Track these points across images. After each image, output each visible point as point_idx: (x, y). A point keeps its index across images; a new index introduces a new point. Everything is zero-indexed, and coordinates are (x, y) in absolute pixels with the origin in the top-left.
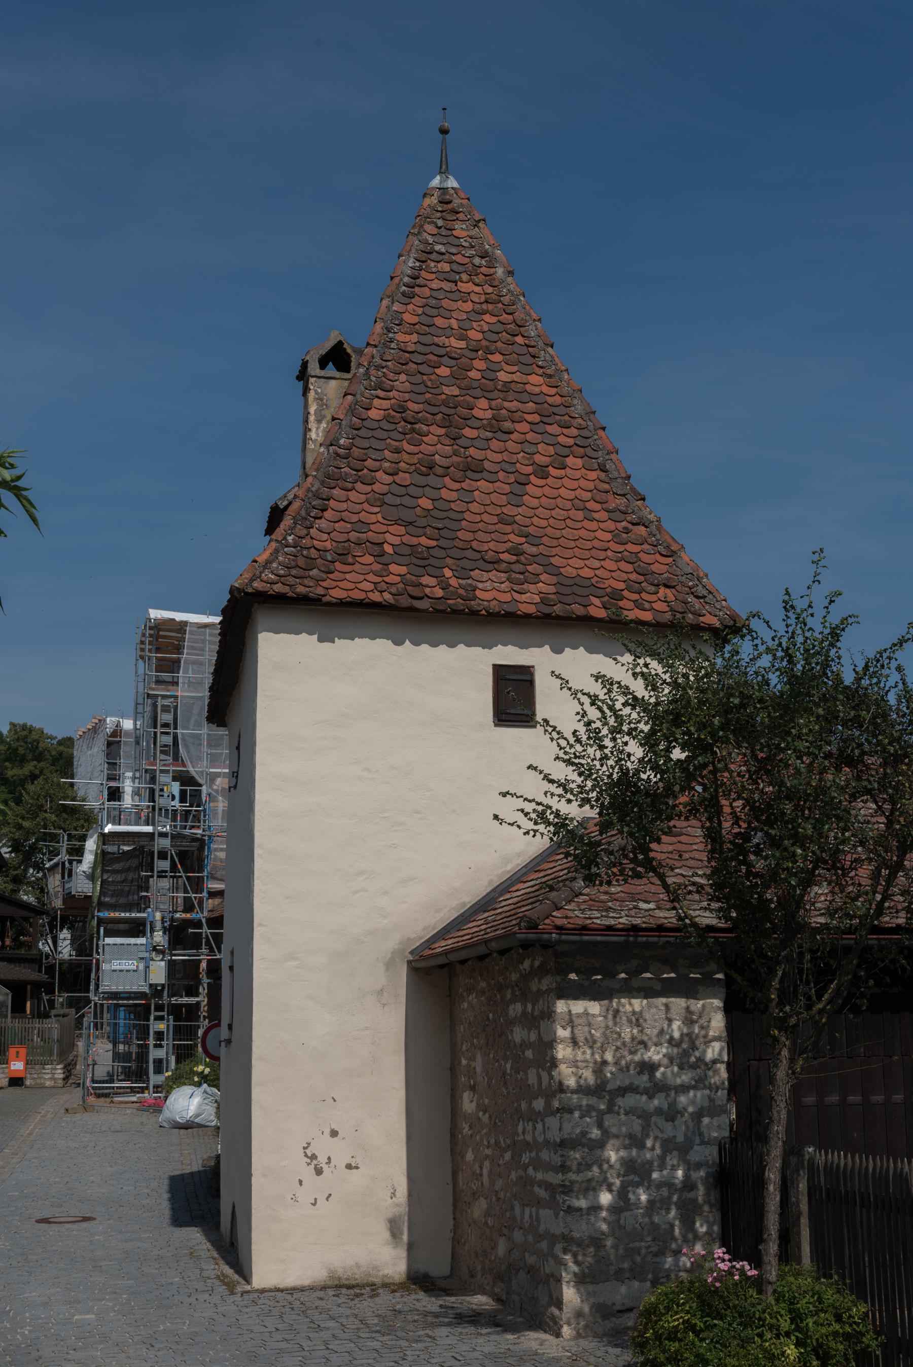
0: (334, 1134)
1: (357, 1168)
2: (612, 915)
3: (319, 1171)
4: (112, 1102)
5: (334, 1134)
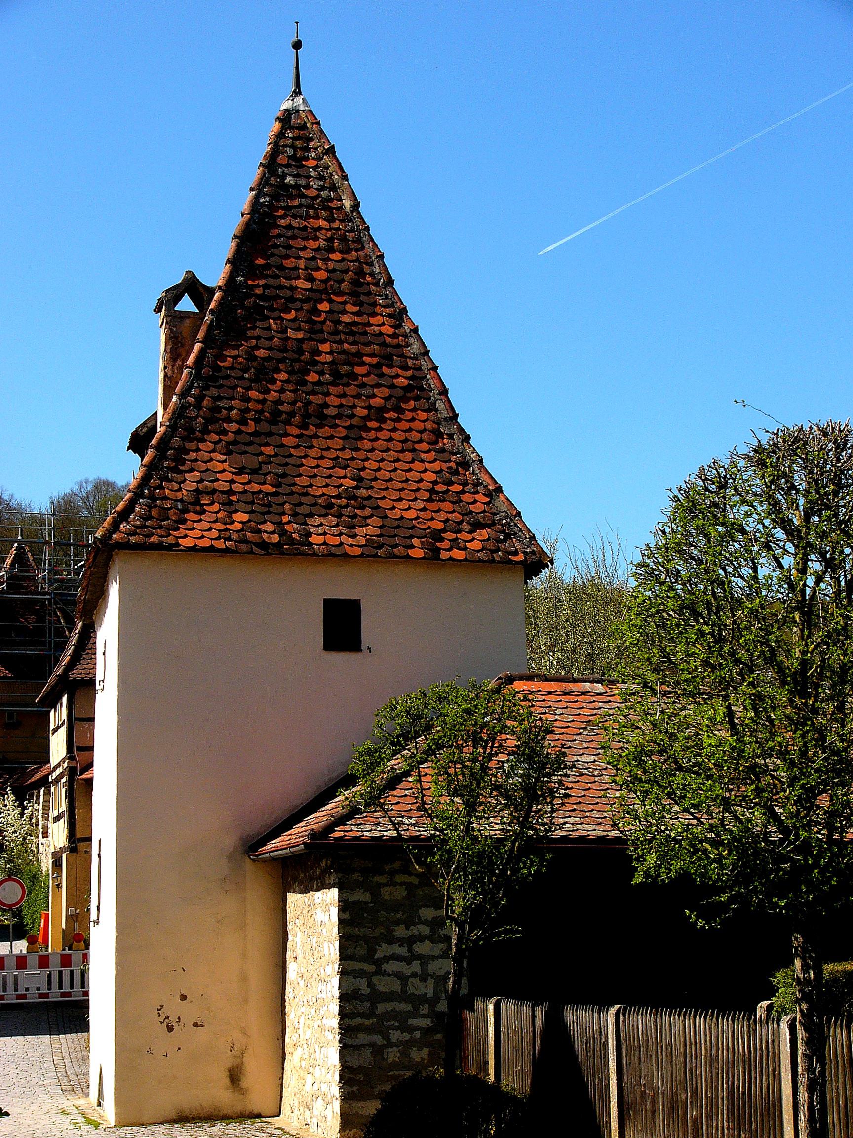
0: (183, 997)
1: (202, 1026)
2: (379, 828)
3: (170, 1029)
4: (97, 922)
5: (183, 997)
